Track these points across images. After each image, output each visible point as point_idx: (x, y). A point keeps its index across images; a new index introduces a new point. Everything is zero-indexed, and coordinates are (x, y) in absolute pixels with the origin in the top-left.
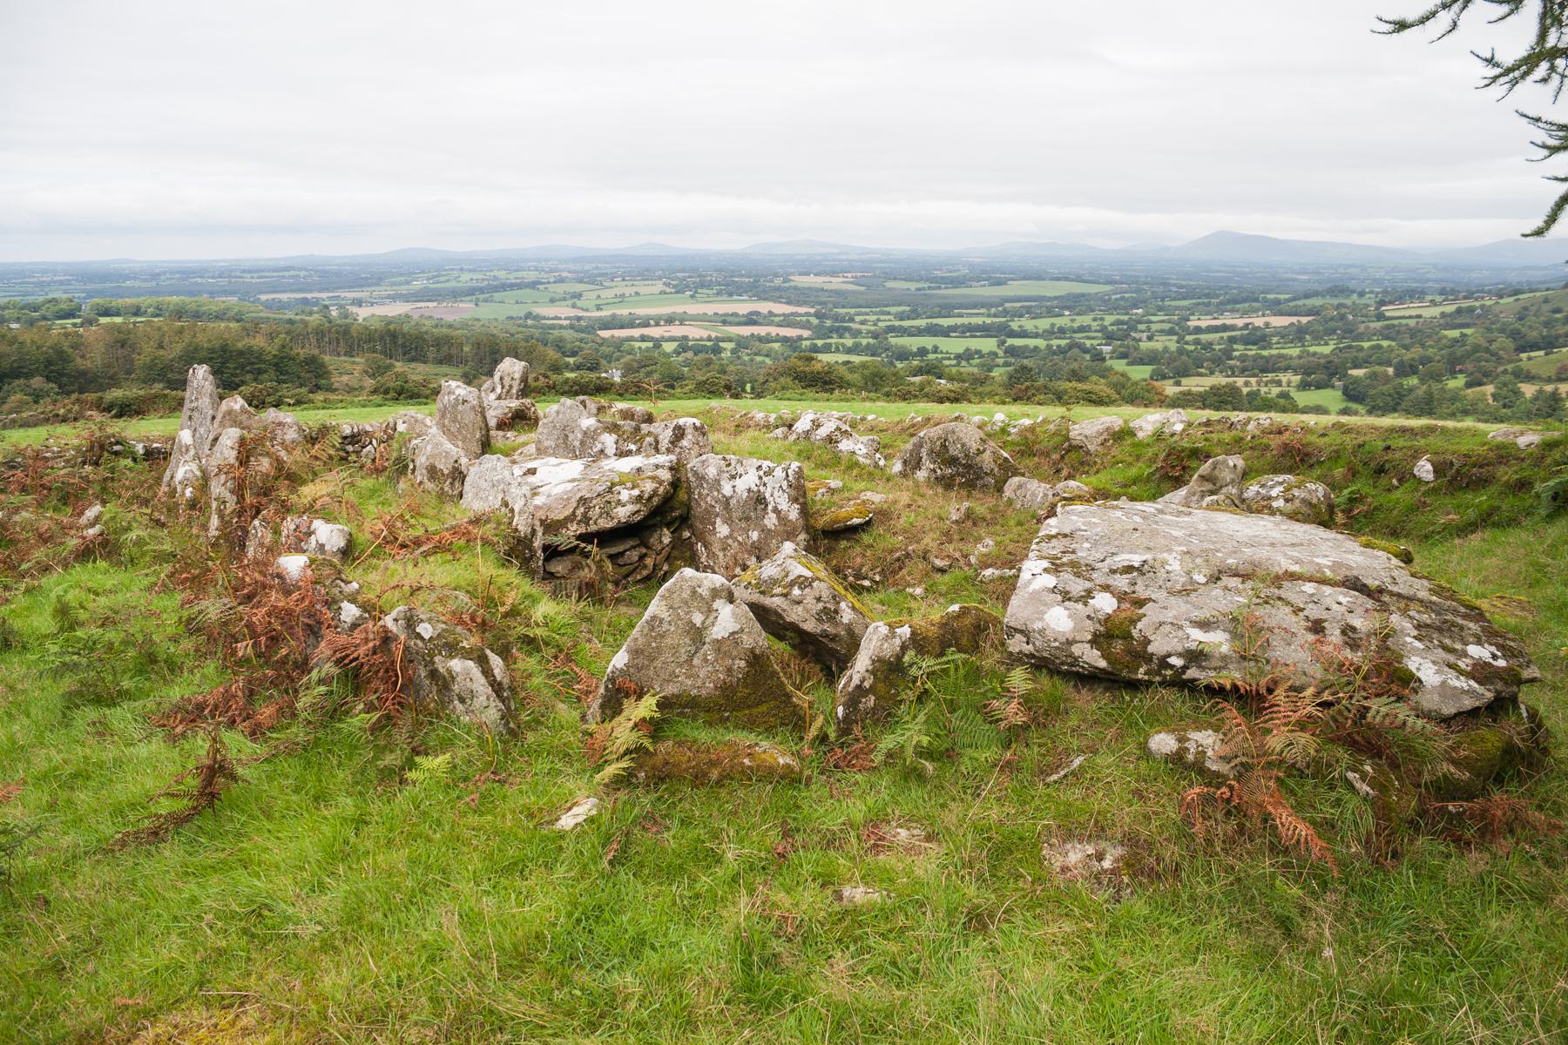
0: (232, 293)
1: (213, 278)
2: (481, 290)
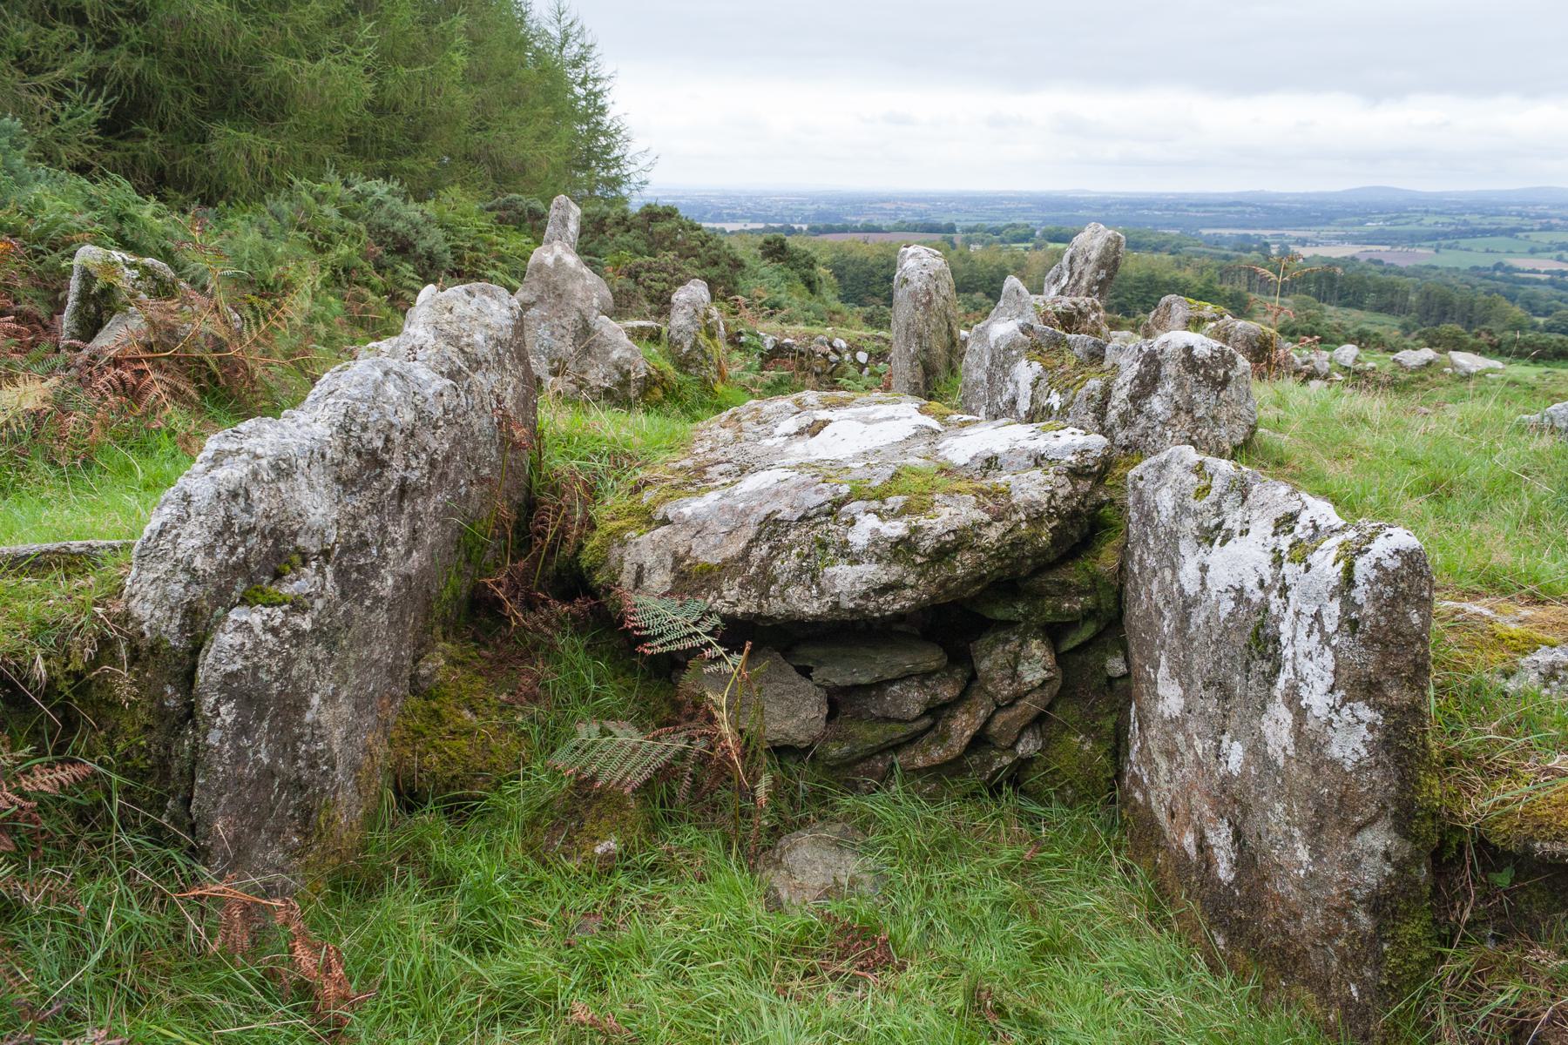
0: (1175, 226)
1: (1159, 210)
2: (1446, 236)
